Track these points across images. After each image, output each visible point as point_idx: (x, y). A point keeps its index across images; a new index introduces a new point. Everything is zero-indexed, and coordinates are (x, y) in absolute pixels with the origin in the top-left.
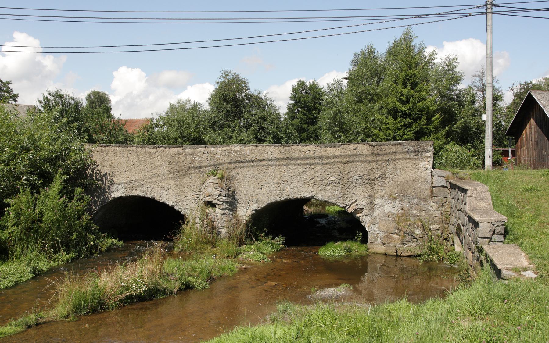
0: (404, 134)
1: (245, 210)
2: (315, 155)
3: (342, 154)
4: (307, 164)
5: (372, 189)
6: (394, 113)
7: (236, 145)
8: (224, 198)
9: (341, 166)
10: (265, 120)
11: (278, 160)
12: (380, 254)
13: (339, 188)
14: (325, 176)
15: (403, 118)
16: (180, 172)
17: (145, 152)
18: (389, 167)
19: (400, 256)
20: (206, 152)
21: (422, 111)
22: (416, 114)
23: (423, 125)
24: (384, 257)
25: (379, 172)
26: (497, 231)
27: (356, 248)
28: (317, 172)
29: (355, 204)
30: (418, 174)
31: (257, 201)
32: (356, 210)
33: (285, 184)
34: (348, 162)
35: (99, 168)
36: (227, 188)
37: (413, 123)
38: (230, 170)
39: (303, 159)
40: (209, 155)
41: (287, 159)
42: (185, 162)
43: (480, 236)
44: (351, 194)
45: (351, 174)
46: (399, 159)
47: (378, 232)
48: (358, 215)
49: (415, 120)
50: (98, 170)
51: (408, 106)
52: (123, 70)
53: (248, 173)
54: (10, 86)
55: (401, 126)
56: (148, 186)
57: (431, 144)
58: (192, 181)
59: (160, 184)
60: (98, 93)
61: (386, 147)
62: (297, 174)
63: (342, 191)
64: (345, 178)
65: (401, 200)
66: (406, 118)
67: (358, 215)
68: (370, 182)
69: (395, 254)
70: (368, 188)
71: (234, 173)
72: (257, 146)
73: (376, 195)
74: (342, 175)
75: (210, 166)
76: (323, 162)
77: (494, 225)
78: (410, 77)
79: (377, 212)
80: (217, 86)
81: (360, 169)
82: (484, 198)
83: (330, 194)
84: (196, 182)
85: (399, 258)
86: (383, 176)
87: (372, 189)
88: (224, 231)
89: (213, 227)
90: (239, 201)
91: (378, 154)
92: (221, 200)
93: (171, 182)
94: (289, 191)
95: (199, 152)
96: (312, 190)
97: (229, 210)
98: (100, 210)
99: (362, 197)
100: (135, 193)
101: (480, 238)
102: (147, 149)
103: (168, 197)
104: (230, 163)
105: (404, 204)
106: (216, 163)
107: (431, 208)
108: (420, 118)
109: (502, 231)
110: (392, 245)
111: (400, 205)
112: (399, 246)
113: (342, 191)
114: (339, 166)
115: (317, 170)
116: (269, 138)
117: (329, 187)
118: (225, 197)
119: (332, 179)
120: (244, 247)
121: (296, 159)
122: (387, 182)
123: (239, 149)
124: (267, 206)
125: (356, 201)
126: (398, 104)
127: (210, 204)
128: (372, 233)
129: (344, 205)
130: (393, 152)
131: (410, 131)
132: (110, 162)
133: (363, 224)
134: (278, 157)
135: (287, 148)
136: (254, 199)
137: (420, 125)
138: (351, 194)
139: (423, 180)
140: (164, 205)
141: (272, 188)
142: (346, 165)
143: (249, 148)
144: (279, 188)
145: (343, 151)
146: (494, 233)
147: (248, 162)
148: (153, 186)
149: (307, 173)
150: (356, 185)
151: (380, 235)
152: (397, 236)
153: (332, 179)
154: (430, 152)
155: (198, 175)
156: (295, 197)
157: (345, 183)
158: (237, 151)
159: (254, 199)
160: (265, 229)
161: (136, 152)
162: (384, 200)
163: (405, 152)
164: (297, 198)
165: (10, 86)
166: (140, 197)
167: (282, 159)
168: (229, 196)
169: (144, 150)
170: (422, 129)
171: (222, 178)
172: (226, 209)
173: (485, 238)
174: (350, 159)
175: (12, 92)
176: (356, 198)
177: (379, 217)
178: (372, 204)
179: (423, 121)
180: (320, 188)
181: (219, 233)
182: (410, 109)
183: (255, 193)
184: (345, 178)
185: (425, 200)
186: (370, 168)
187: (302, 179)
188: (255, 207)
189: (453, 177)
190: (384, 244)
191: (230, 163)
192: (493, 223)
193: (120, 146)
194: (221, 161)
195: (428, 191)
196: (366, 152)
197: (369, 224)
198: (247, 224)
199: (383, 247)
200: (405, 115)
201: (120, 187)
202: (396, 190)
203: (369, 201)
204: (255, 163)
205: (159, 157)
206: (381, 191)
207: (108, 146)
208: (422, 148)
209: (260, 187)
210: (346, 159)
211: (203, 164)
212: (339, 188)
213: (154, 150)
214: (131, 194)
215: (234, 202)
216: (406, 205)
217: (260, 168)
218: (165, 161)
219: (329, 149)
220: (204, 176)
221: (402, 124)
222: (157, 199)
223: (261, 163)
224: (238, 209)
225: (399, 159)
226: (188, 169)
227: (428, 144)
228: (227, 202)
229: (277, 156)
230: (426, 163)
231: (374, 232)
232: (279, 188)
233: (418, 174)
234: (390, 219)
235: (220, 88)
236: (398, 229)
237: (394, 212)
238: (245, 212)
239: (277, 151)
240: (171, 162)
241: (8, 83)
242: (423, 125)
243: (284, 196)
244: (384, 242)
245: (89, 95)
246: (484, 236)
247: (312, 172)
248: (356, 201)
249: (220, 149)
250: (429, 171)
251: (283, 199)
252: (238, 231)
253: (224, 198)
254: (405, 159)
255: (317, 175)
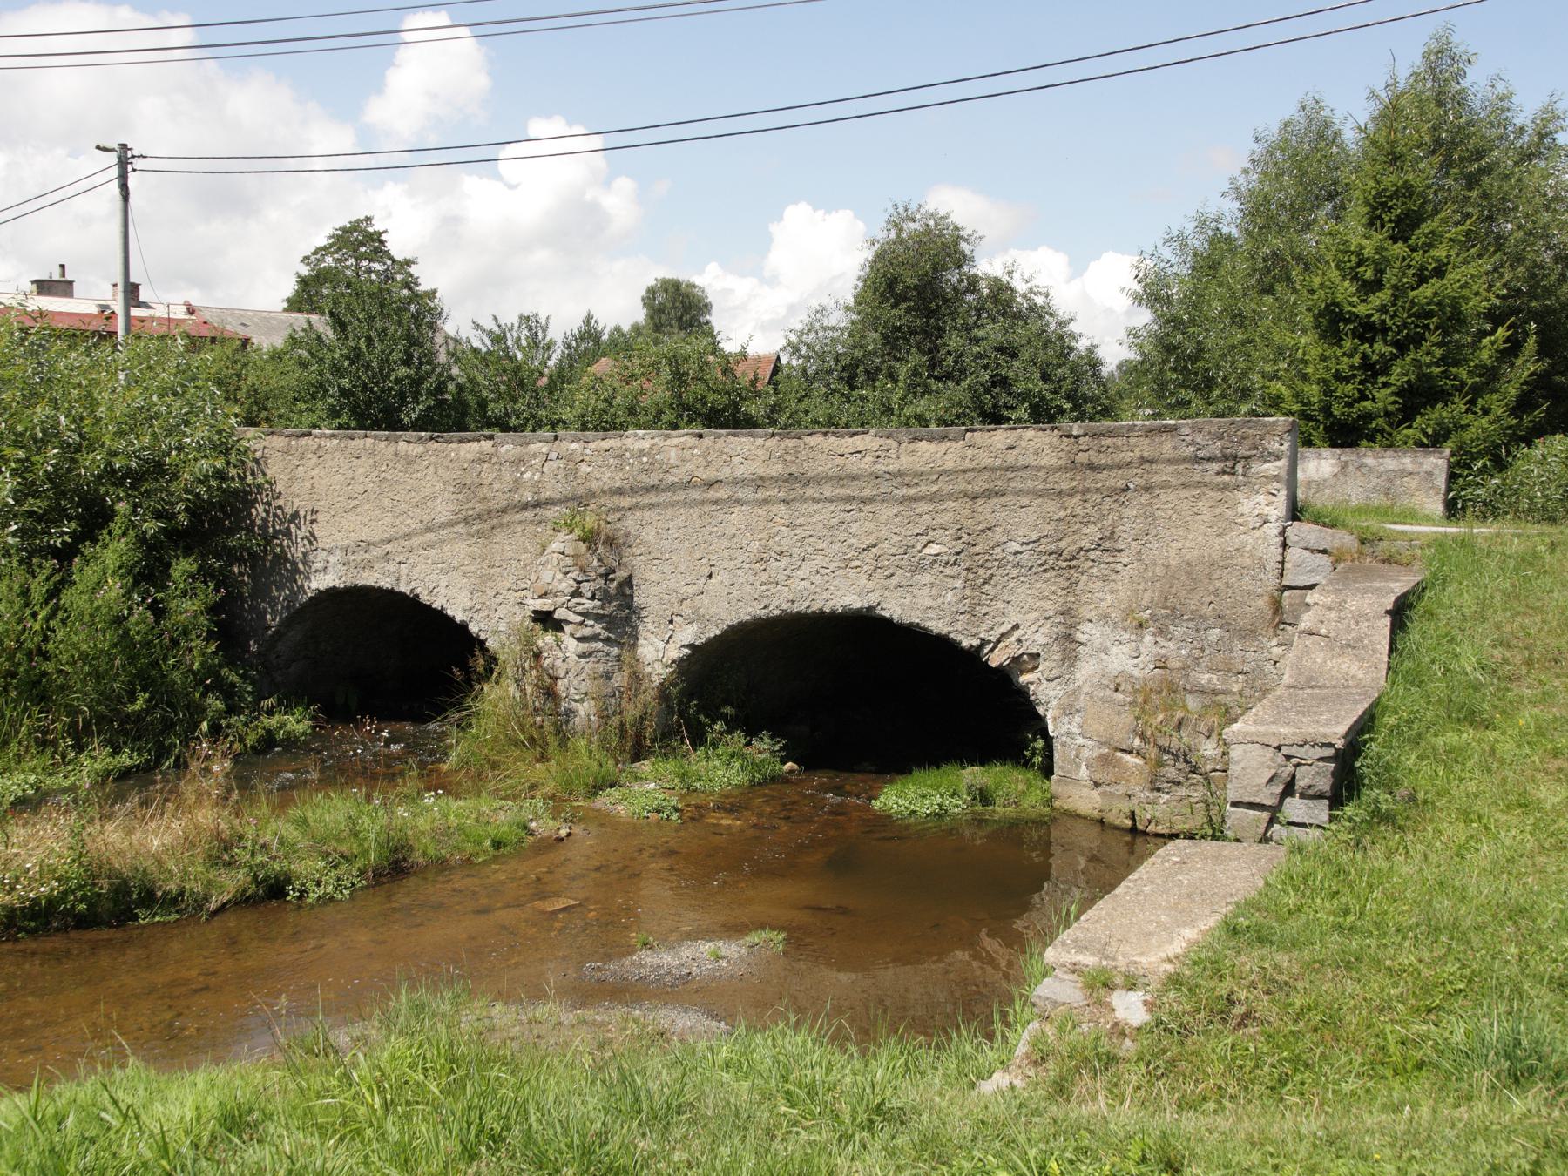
0: (1364, 397)
1: (662, 645)
2: (880, 467)
3: (967, 464)
4: (850, 499)
5: (1070, 587)
6: (1332, 322)
7: (641, 433)
8: (589, 605)
9: (964, 507)
10: (1014, 356)
11: (759, 482)
12: (1085, 818)
13: (959, 583)
14: (912, 541)
15: (1363, 340)
16: (484, 519)
17: (396, 455)
18: (1127, 512)
19: (1145, 833)
20: (553, 455)
21: (1430, 314)
22: (1405, 325)
23: (1429, 366)
24: (1096, 829)
25: (1091, 529)
26: (1301, 784)
27: (1011, 788)
28: (884, 525)
29: (1013, 639)
30: (1233, 539)
31: (697, 618)
32: (1016, 659)
33: (784, 562)
34: (988, 494)
35: (280, 502)
36: (602, 570)
37: (1395, 357)
38: (618, 515)
39: (839, 479)
40: (561, 464)
41: (790, 478)
42: (498, 486)
43: (1232, 795)
44: (1000, 605)
45: (998, 535)
46: (1165, 486)
47: (1080, 741)
48: (1023, 679)
49: (1402, 347)
50: (280, 508)
51: (1384, 296)
52: (798, 214)
53: (671, 524)
54: (413, 270)
55: (1352, 367)
56: (401, 558)
57: (1280, 429)
58: (514, 543)
59: (432, 552)
60: (676, 285)
61: (1119, 441)
62: (820, 530)
63: (968, 592)
64: (977, 549)
65: (1161, 632)
66: (1371, 342)
67: (1023, 679)
68: (1064, 563)
69: (1128, 823)
70: (1050, 586)
71: (631, 523)
72: (700, 436)
73: (1085, 612)
74: (966, 538)
75: (563, 501)
76: (905, 491)
77: (1288, 758)
78: (1391, 198)
79: (1085, 671)
80: (869, 254)
81: (1030, 516)
82: (1360, 639)
83: (929, 603)
84: (526, 551)
85: (1139, 840)
86: (1107, 544)
87: (1070, 587)
88: (585, 711)
89: (550, 694)
90: (644, 613)
91: (1092, 467)
92: (579, 609)
93: (461, 548)
94: (796, 585)
95: (535, 456)
96: (871, 585)
97: (607, 641)
98: (287, 624)
99: (1035, 615)
100: (369, 579)
101: (1234, 804)
102: (401, 443)
103: (452, 599)
104: (620, 492)
105: (1172, 645)
106: (582, 491)
107: (1268, 667)
108: (1418, 340)
109: (1324, 784)
110: (1121, 789)
111: (1156, 650)
112: (1142, 794)
113: (968, 592)
114: (957, 504)
115: (883, 518)
116: (1022, 412)
117: (926, 578)
118: (593, 598)
119: (934, 549)
120: (645, 767)
121: (818, 480)
122: (1119, 567)
123: (646, 444)
124: (725, 633)
125: (1016, 627)
126: (1348, 288)
127: (545, 619)
128: (1064, 744)
129: (976, 642)
130: (1143, 460)
131: (1385, 385)
132: (308, 485)
133: (1041, 710)
134: (761, 471)
135: (791, 443)
136: (686, 609)
137: (1417, 363)
138: (1000, 605)
139: (1248, 562)
140: (440, 616)
141: (743, 577)
142: (980, 501)
143: (675, 441)
144: (764, 577)
145: (970, 452)
146: (1289, 789)
147: (672, 487)
148: (413, 558)
149: (854, 528)
150: (1015, 573)
151: (1085, 753)
152: (1137, 760)
153: (934, 549)
154: (1278, 458)
155: (530, 528)
156: (816, 607)
157: (975, 564)
158: (642, 453)
159: (686, 609)
160: (728, 710)
161: (373, 454)
162: (1107, 630)
163: (1185, 460)
164: (823, 612)
165: (413, 270)
166: (380, 589)
167: (775, 480)
168: (606, 598)
169: (392, 449)
170: (1423, 377)
171: (590, 538)
172: (595, 638)
173: (1252, 806)
174: (992, 487)
175: (417, 284)
176: (1013, 618)
177: (1086, 689)
178: (1068, 641)
179: (1429, 352)
180: (894, 581)
181: (570, 712)
182: (1383, 309)
183: (690, 589)
184: (977, 549)
185: (1250, 634)
186: (1062, 514)
187: (836, 547)
188: (689, 634)
189: (1360, 553)
190: (1097, 785)
191: (620, 492)
192: (1285, 750)
193: (333, 436)
194: (594, 485)
195: (1263, 603)
196: (1049, 459)
197: (1057, 713)
198: (663, 693)
199: (1095, 793)
200: (1367, 330)
201: (332, 559)
202: (1147, 596)
203: (1061, 629)
204: (695, 495)
205: (431, 468)
206: (1105, 594)
207: (304, 435)
208: (1247, 443)
209: (707, 572)
210: (979, 485)
211: (546, 494)
212: (959, 583)
213: (419, 449)
214: (361, 582)
215: (628, 619)
216: (1175, 650)
217: (707, 508)
218: (445, 483)
219: (924, 445)
220: (544, 531)
221: (1357, 360)
222: (425, 598)
223: (712, 494)
224: (641, 641)
225: (1165, 486)
226: (504, 511)
227: (1270, 431)
228: (599, 618)
229: (756, 468)
230: (1261, 498)
231: (1069, 740)
232: (764, 577)
233: (1233, 539)
234: (1119, 697)
235: (879, 256)
236: (1143, 737)
237: (1136, 672)
238: (659, 651)
239: (760, 452)
240: (461, 486)
241: (408, 263)
242: (1429, 366)
243: (779, 603)
244: (1097, 777)
245: (652, 292)
246: (1246, 799)
247: (869, 526)
248: (1016, 627)
249: (592, 445)
250: (1272, 529)
251: (777, 612)
252: (632, 713)
253: (589, 605)
254: (1185, 486)
255: (884, 534)
